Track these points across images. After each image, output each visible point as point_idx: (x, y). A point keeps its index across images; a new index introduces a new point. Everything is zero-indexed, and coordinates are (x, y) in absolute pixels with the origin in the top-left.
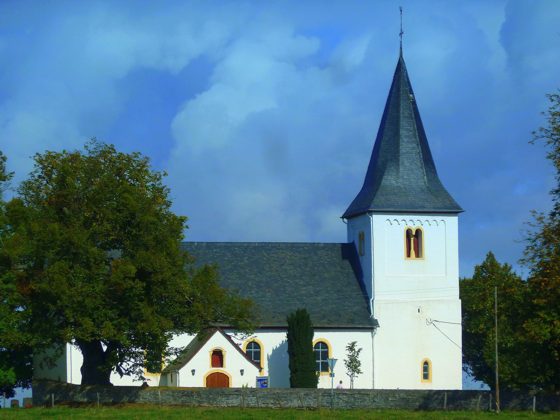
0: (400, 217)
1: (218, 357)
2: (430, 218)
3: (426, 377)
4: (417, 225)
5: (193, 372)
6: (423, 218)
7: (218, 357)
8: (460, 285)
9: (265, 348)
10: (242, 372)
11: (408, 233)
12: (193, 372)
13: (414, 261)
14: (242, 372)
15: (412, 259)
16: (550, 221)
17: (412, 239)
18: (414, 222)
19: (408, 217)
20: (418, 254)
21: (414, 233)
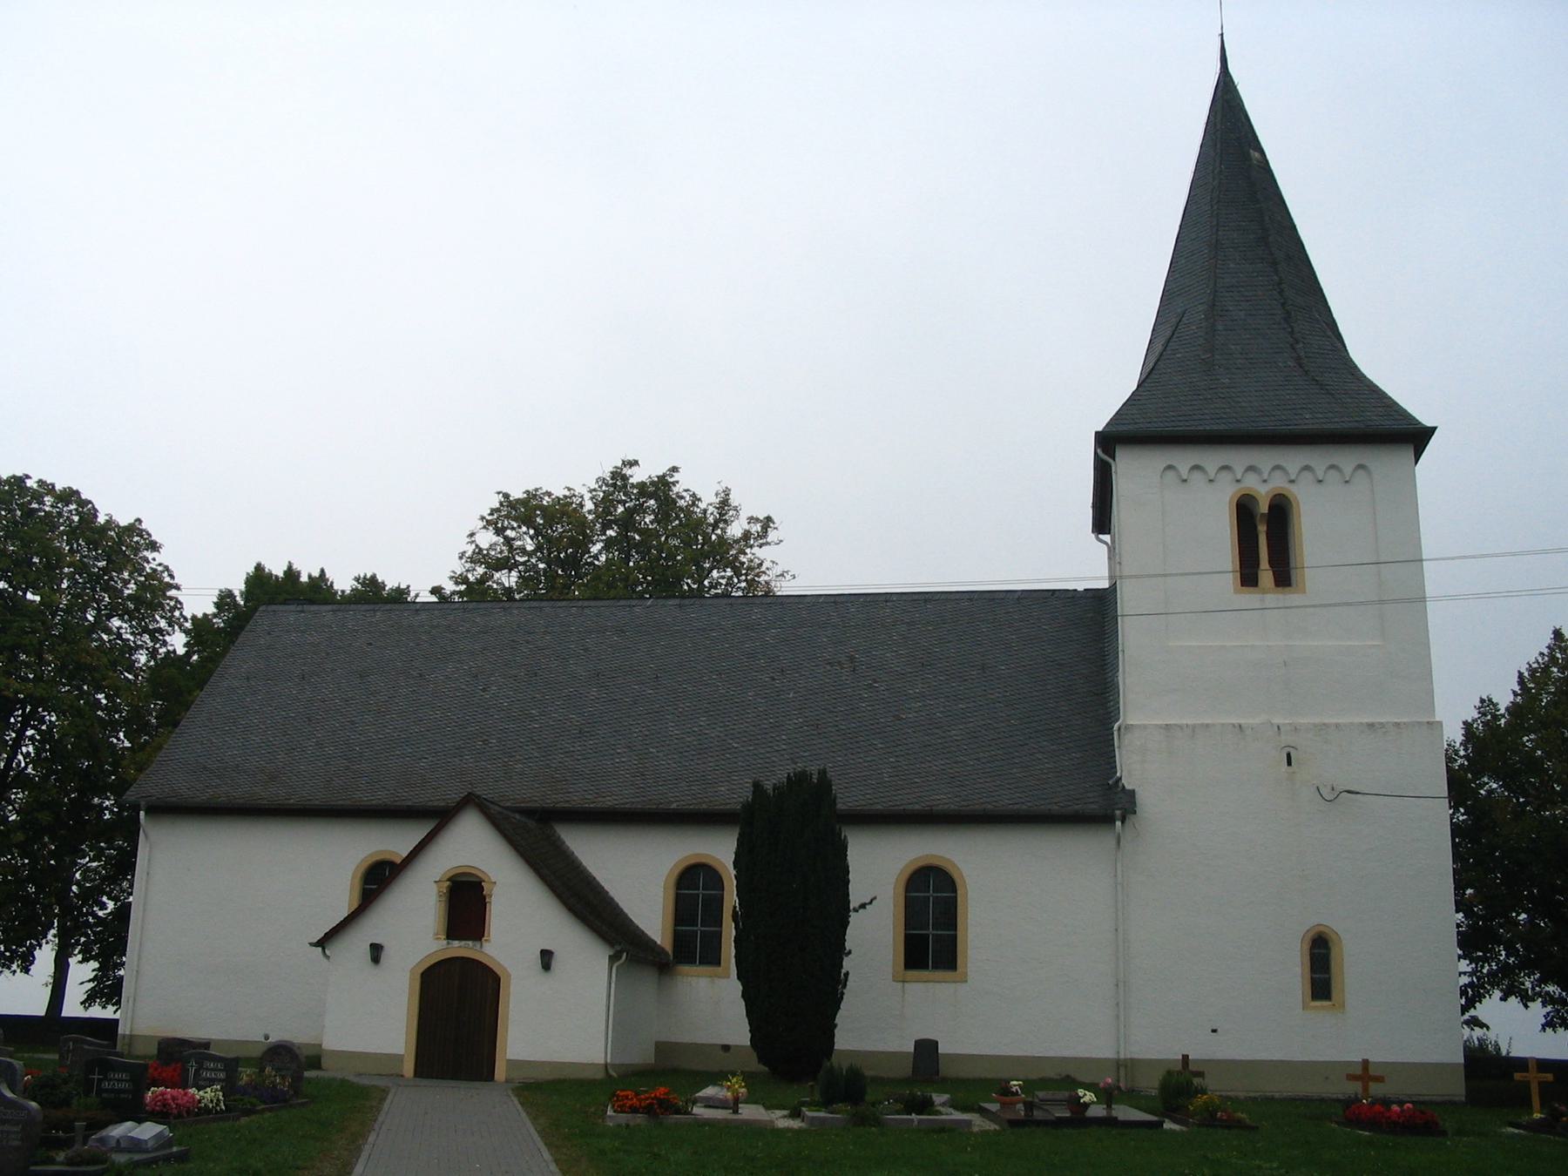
0: (1211, 459)
1: (466, 904)
2: (1319, 458)
3: (1321, 985)
4: (1278, 483)
5: (376, 952)
6: (1293, 459)
7: (466, 904)
8: (428, 1077)
9: (666, 871)
10: (546, 958)
11: (1244, 510)
12: (376, 952)
13: (1268, 597)
14: (546, 958)
15: (1264, 592)
16: (514, 573)
17: (1262, 529)
18: (1265, 473)
19: (1240, 458)
20: (1284, 579)
21: (1264, 508)
